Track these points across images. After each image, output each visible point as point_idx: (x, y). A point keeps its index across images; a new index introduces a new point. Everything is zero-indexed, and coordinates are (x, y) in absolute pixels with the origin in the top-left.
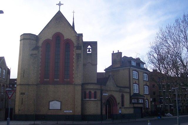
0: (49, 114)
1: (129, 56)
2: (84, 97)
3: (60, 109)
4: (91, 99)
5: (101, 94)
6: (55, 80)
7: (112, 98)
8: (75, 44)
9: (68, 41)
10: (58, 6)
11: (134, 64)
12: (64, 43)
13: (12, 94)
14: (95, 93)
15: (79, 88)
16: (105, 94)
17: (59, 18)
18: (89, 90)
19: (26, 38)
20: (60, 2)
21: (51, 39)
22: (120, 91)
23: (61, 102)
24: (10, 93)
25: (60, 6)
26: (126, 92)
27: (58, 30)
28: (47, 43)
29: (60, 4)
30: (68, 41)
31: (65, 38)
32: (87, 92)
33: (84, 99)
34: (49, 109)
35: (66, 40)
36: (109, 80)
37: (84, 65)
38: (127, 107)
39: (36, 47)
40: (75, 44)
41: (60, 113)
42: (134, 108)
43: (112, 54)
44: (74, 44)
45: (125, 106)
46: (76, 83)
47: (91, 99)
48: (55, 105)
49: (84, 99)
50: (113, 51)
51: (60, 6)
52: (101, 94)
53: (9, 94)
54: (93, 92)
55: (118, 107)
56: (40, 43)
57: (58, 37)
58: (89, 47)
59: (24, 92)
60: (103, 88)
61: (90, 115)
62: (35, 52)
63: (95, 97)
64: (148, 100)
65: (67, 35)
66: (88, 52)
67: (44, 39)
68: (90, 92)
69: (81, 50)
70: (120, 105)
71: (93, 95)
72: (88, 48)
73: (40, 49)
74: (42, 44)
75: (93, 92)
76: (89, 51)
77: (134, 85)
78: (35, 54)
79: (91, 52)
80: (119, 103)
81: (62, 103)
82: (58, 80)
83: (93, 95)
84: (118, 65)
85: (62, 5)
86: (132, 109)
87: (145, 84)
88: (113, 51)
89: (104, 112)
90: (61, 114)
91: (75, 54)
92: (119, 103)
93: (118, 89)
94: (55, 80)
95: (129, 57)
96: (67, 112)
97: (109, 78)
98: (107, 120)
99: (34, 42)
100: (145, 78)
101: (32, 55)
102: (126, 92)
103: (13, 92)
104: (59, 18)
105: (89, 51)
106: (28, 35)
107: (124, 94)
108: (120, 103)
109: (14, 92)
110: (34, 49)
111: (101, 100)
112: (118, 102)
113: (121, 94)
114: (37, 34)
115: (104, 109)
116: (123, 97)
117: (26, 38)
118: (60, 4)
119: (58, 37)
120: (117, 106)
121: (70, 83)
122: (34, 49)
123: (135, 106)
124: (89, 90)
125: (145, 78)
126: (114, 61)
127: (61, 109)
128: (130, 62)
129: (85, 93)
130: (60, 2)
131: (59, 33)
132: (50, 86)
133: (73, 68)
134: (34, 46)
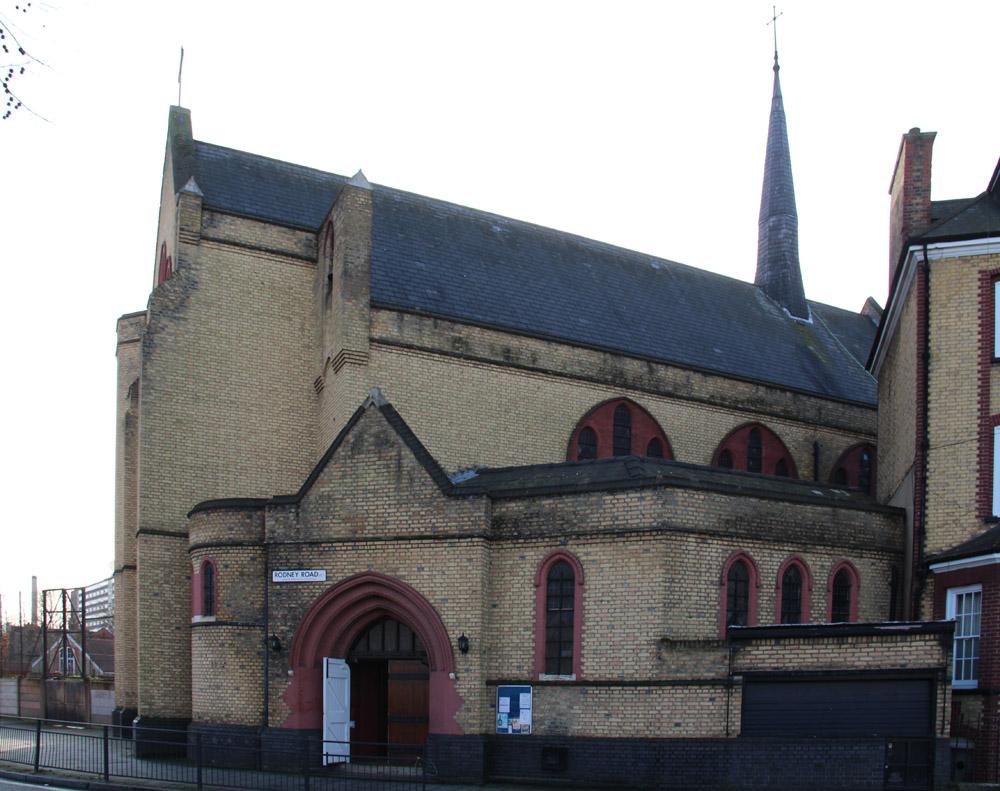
16: (298, 576)
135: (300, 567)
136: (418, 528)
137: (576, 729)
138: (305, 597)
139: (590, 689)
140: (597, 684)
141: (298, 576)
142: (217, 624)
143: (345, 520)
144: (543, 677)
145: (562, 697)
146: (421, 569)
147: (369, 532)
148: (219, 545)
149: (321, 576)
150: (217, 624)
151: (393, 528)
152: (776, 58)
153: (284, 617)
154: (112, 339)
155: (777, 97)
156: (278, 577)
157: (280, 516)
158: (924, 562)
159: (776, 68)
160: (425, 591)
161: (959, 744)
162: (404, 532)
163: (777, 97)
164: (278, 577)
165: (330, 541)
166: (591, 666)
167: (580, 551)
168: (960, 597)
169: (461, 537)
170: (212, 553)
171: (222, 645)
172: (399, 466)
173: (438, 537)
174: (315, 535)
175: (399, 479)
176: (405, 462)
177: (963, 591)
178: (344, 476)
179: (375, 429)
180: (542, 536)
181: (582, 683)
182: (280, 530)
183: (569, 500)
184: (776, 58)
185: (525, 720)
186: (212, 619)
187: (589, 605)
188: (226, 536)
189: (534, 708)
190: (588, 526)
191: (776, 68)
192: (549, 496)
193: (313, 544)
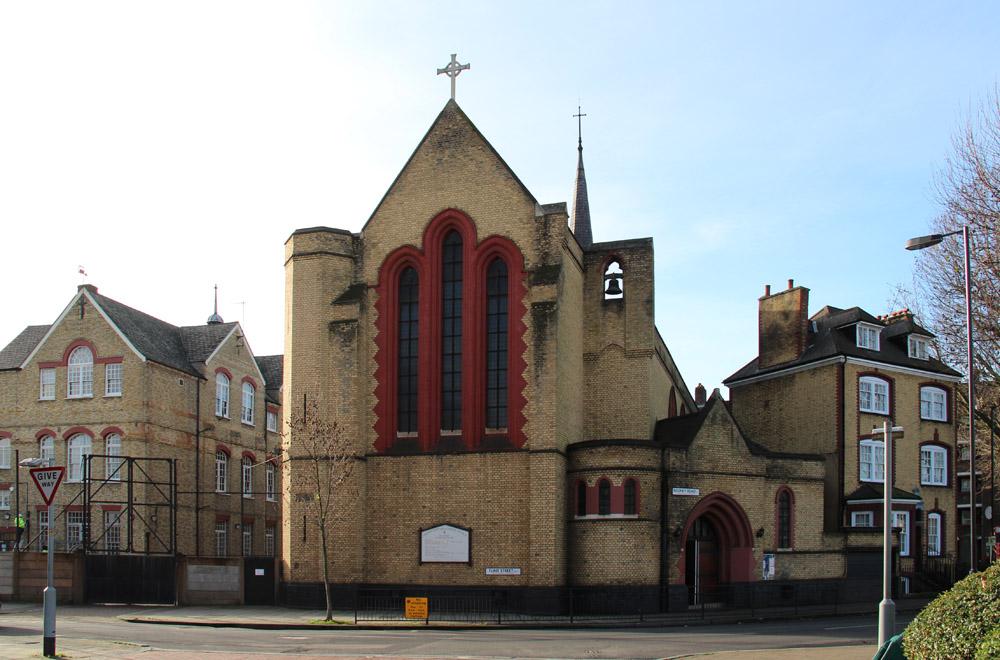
0: (421, 582)
1: (844, 304)
2: (576, 509)
3: (466, 560)
4: (607, 517)
5: (665, 490)
6: (444, 433)
7: (723, 505)
8: (531, 258)
9: (496, 248)
10: (445, 78)
11: (869, 339)
12: (480, 255)
13: (56, 481)
14: (631, 485)
15: (551, 469)
16: (685, 492)
17: (452, 134)
18: (599, 475)
19: (315, 247)
20: (454, 56)
21: (418, 243)
22: (769, 476)
23: (470, 531)
24: (47, 480)
25: (453, 77)
26: (808, 480)
27: (454, 196)
28: (402, 264)
29: (453, 69)
30: (496, 248)
31: (482, 235)
32: (593, 481)
33: (576, 517)
34: (421, 563)
35: (486, 240)
36: (707, 422)
37: (590, 358)
38: (807, 547)
39: (351, 287)
40: (531, 258)
41: (469, 579)
42: (848, 551)
43: (762, 300)
44: (523, 257)
45: (798, 545)
46: (534, 445)
47: (607, 517)
48: (446, 546)
49: (576, 517)
50: (768, 287)
51: (453, 77)
52: (665, 490)
53: (44, 484)
54: (617, 481)
55: (757, 552)
56: (370, 273)
57: (449, 229)
58: (614, 268)
59: (308, 489)
60: (674, 459)
61: (601, 589)
62: (350, 311)
63: (631, 505)
64: (943, 515)
65: (491, 220)
66: (608, 297)
67: (388, 250)
68: (605, 485)
69: (555, 286)
70: (770, 540)
71: (617, 499)
72: (607, 273)
73: (372, 297)
74: (381, 270)
75: (617, 481)
76: (614, 289)
77: (862, 443)
78: (347, 322)
79: (620, 296)
80: (762, 530)
81: (474, 539)
82: (458, 433)
83: (617, 499)
84: (789, 356)
85: (444, 67)
86: (837, 556)
87: (931, 437)
88: (768, 287)
89: (676, 576)
90: (471, 581)
91: (527, 303)
92: (762, 530)
93: (760, 464)
94: (444, 433)
95: (845, 308)
96: (500, 572)
97: (710, 414)
98: (690, 607)
99: (344, 265)
100: (874, 398)
101: (334, 326)
102: (808, 480)
103: (59, 472)
104: (452, 134)
105: (614, 289)
106: (315, 235)
107: (798, 489)
108: (771, 531)
109: (61, 476)
110: (342, 300)
111: (664, 517)
112: (755, 527)
113: (774, 487)
114: (356, 228)
115: (677, 560)
116: (786, 501)
117: (315, 247)
118: (453, 69)
119: (449, 229)
120: (749, 544)
121: (512, 443)
122: (342, 300)
123: (854, 544)
124: (599, 475)
125: (874, 398)
126: (769, 338)
127: (470, 563)
128: (849, 333)
129: (583, 485)
130: (454, 56)
131: (455, 210)
132: (423, 460)
133: (524, 375)
134: (346, 284)
135: (687, 486)
136: (741, 469)
137: (792, 575)
138: (690, 504)
139: (799, 556)
140: (800, 553)
141: (685, 492)
142: (639, 520)
143: (710, 461)
144: (779, 550)
145: (787, 558)
146: (740, 492)
147: (720, 470)
148: (642, 469)
149: (697, 492)
150: (639, 520)
151: (730, 469)
152: (580, 142)
153: (678, 516)
154: (284, 252)
155: (581, 169)
156: (676, 491)
157: (679, 455)
158: (843, 499)
159: (580, 149)
160: (741, 504)
161: (353, 619)
162: (735, 471)
163: (581, 169)
164: (676, 491)
165: (703, 472)
166: (798, 545)
167: (791, 486)
168: (857, 516)
169: (757, 476)
170: (635, 474)
171: (643, 534)
172: (732, 434)
173: (749, 475)
174: (696, 469)
175: (732, 442)
176: (734, 433)
177: (858, 513)
178: (708, 437)
179: (721, 412)
180: (779, 478)
181: (794, 552)
182: (678, 464)
183: (789, 461)
184: (580, 142)
185: (772, 571)
186: (636, 516)
187: (797, 513)
188: (647, 464)
189: (776, 566)
190: (796, 475)
191: (580, 149)
192: (781, 458)
193: (695, 473)
